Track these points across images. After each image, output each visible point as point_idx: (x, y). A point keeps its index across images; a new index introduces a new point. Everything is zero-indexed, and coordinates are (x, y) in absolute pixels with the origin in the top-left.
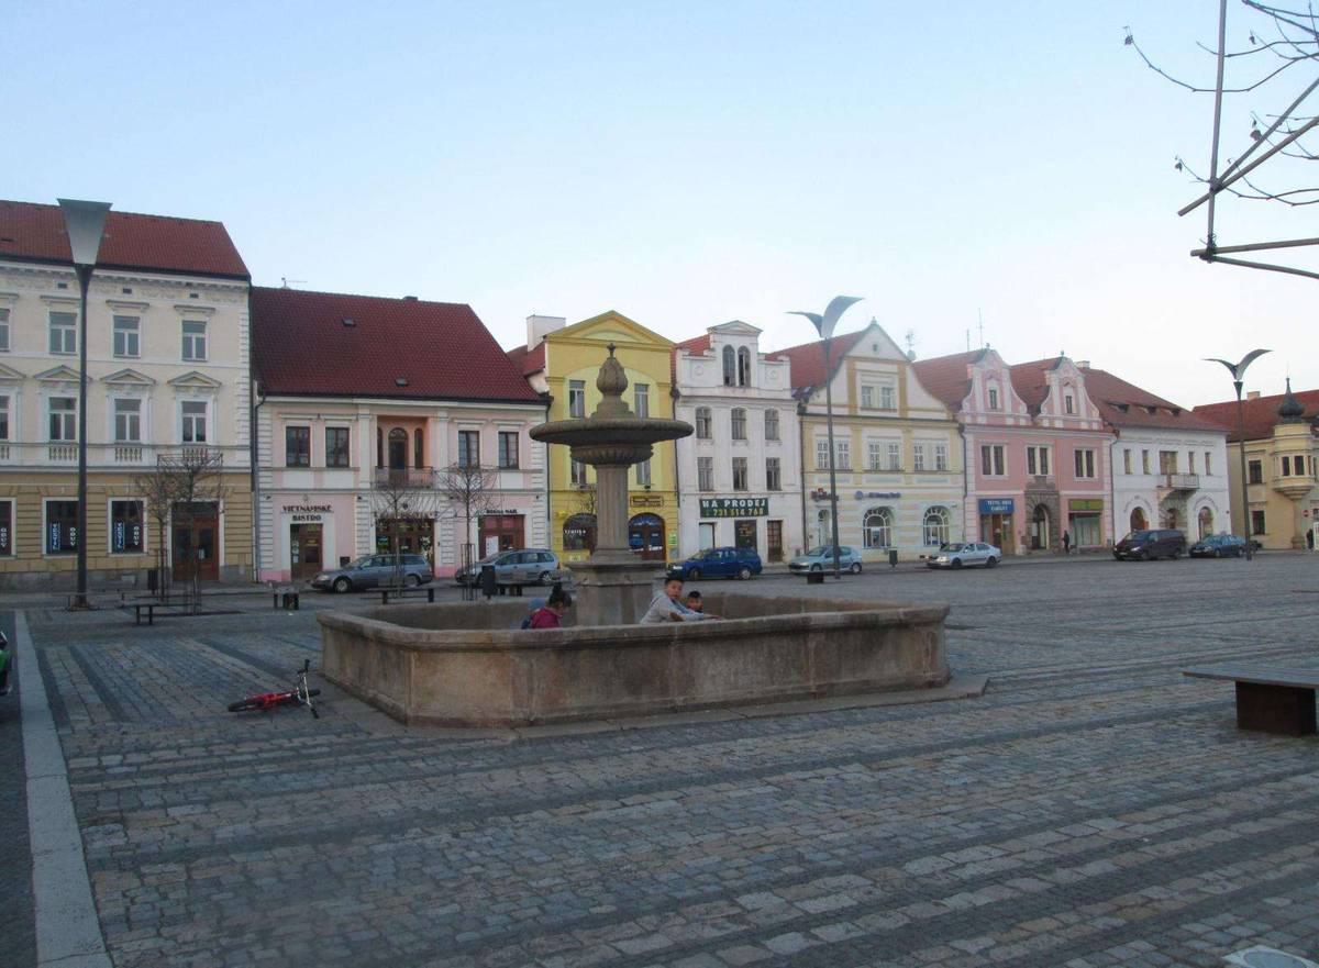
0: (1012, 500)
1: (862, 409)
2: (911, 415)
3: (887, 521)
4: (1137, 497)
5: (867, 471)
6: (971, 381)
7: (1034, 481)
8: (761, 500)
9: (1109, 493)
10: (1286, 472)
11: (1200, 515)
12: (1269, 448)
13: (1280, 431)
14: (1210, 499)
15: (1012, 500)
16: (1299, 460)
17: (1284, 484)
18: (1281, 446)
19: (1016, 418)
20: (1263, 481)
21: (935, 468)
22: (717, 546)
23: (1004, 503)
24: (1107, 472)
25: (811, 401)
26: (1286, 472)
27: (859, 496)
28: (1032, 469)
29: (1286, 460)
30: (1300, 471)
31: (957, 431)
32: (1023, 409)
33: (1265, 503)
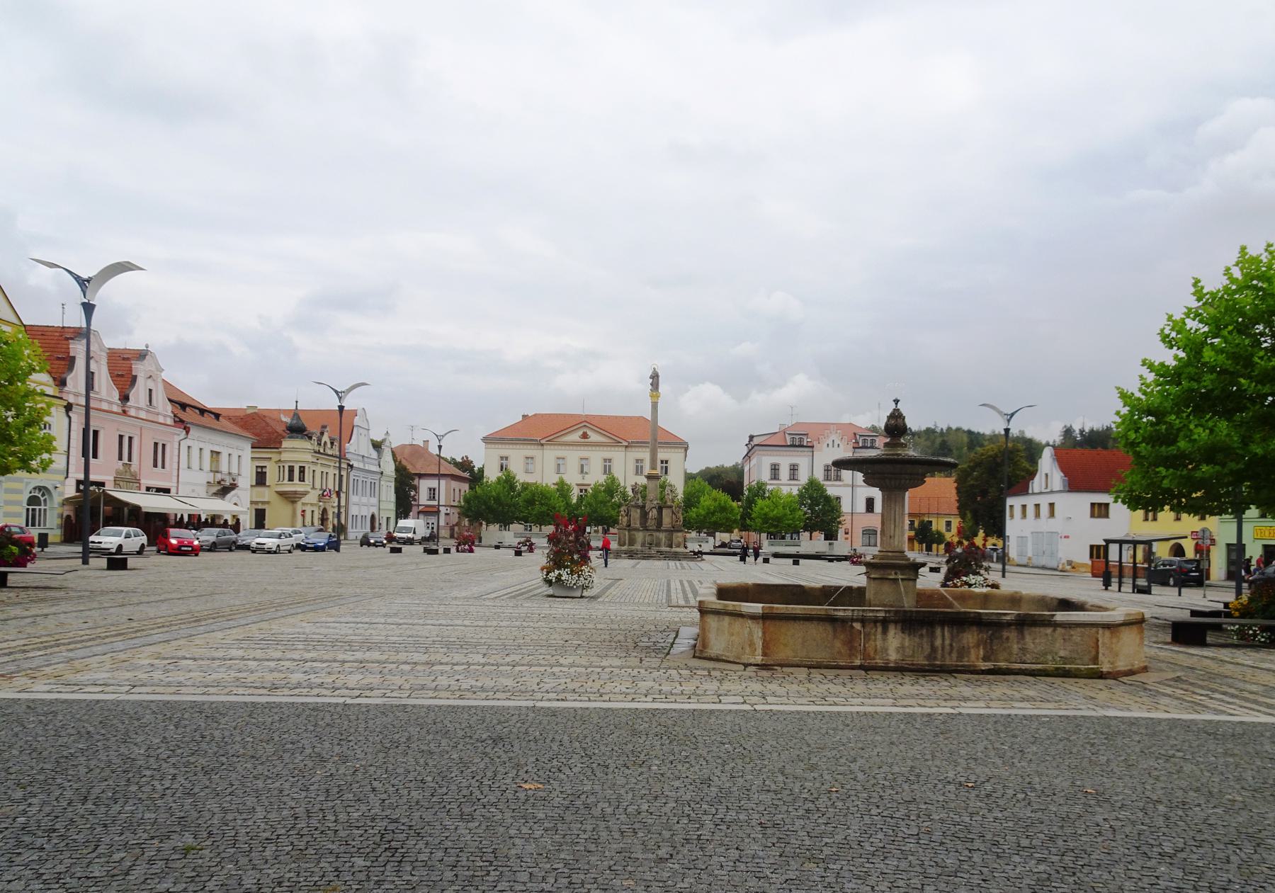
3: (45, 500)
6: (74, 358)
7: (121, 468)
9: (176, 485)
10: (291, 479)
12: (275, 457)
13: (287, 444)
16: (302, 470)
17: (288, 487)
18: (285, 456)
19: (111, 403)
20: (267, 484)
22: (1177, 589)
26: (291, 479)
28: (120, 458)
29: (291, 470)
30: (302, 479)
31: (64, 410)
32: (116, 395)
33: (268, 503)
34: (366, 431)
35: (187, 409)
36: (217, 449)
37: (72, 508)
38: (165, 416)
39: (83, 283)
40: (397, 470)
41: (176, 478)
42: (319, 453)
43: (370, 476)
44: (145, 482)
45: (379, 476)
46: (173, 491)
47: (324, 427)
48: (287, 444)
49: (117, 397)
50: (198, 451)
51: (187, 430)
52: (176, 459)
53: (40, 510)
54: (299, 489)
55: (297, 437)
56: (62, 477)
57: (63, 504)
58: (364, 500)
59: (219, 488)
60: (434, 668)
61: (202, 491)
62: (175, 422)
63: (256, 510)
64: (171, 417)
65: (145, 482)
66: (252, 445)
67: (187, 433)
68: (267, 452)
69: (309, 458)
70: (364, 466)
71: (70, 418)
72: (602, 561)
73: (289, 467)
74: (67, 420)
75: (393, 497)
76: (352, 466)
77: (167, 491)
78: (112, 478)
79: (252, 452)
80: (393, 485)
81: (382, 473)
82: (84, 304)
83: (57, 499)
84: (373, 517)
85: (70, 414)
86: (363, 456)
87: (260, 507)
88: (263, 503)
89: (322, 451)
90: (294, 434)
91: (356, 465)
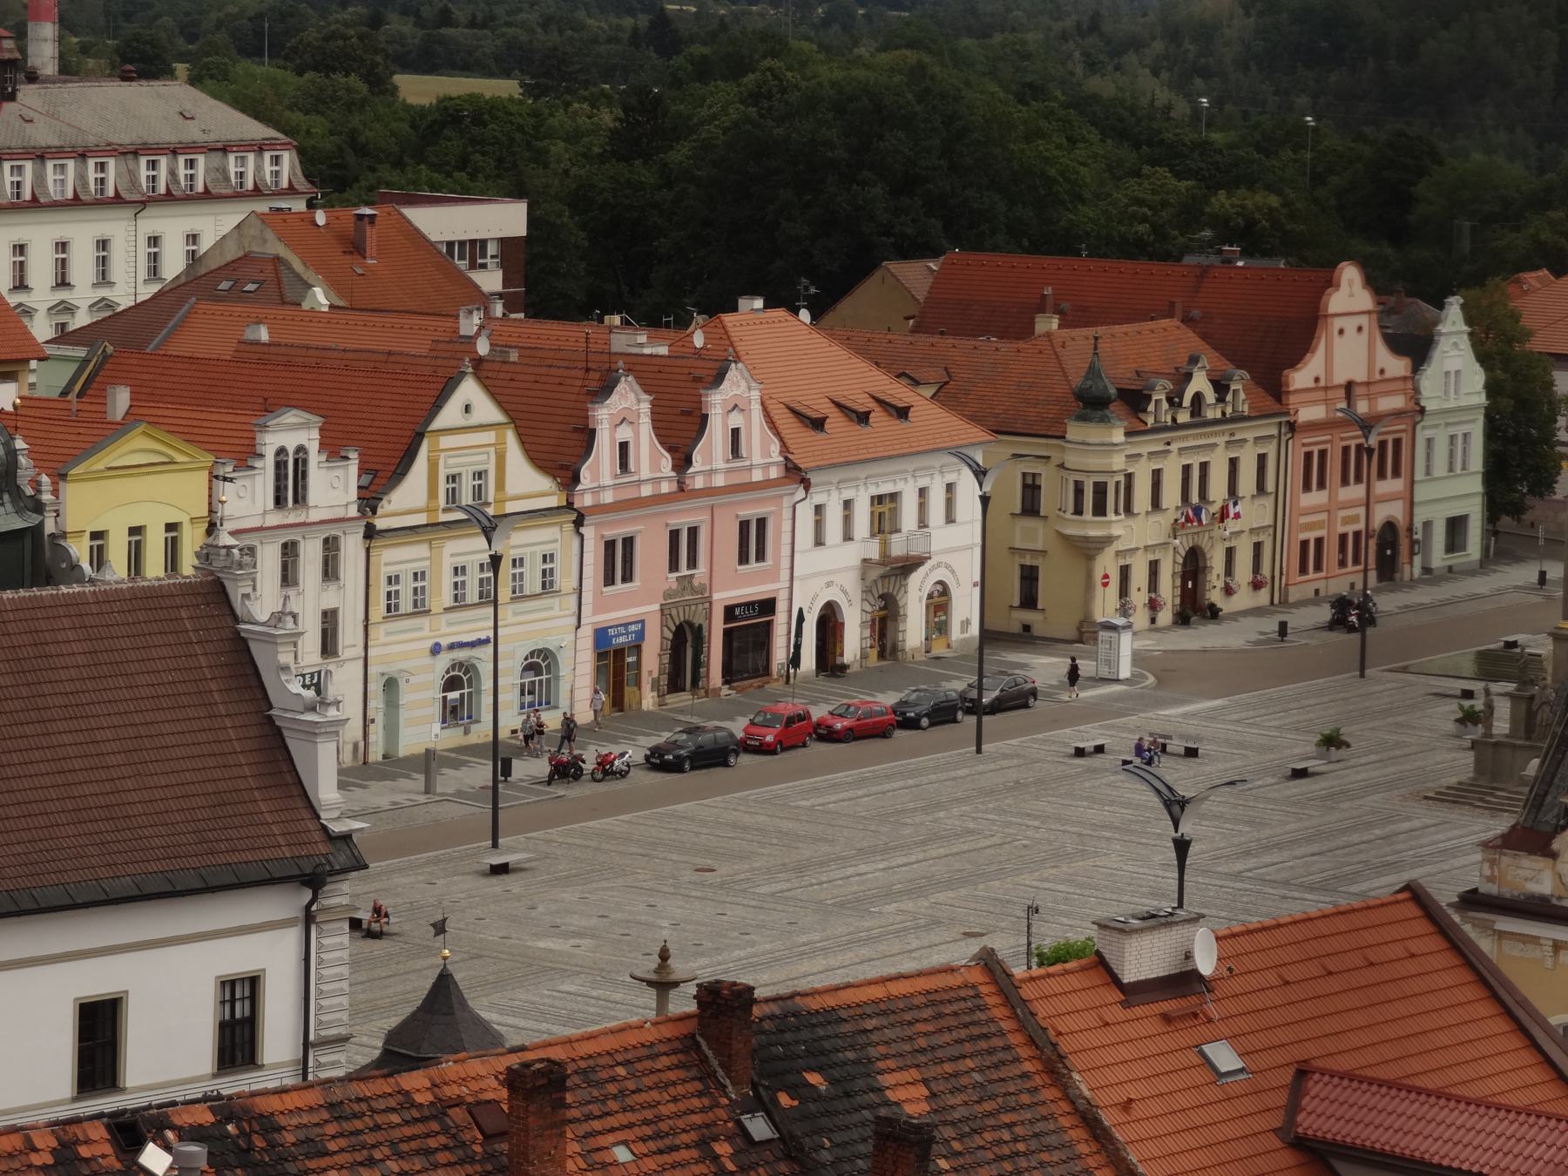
0: (642, 622)
1: (445, 510)
2: (511, 507)
4: (829, 585)
5: (448, 610)
8: (312, 674)
10: (1078, 511)
11: (930, 596)
14: (947, 567)
15: (642, 622)
21: (539, 590)
23: (633, 628)
25: (380, 511)
26: (1078, 511)
27: (436, 650)
28: (674, 565)
30: (1100, 509)
32: (666, 462)
36: (886, 488)
51: (807, 485)
52: (786, 538)
53: (541, 681)
54: (1092, 533)
60: (1240, 203)
63: (1022, 567)
67: (807, 489)
68: (758, 500)
71: (582, 536)
73: (1096, 484)
74: (576, 542)
78: (657, 607)
85: (582, 530)
87: (1028, 561)
88: (1034, 552)
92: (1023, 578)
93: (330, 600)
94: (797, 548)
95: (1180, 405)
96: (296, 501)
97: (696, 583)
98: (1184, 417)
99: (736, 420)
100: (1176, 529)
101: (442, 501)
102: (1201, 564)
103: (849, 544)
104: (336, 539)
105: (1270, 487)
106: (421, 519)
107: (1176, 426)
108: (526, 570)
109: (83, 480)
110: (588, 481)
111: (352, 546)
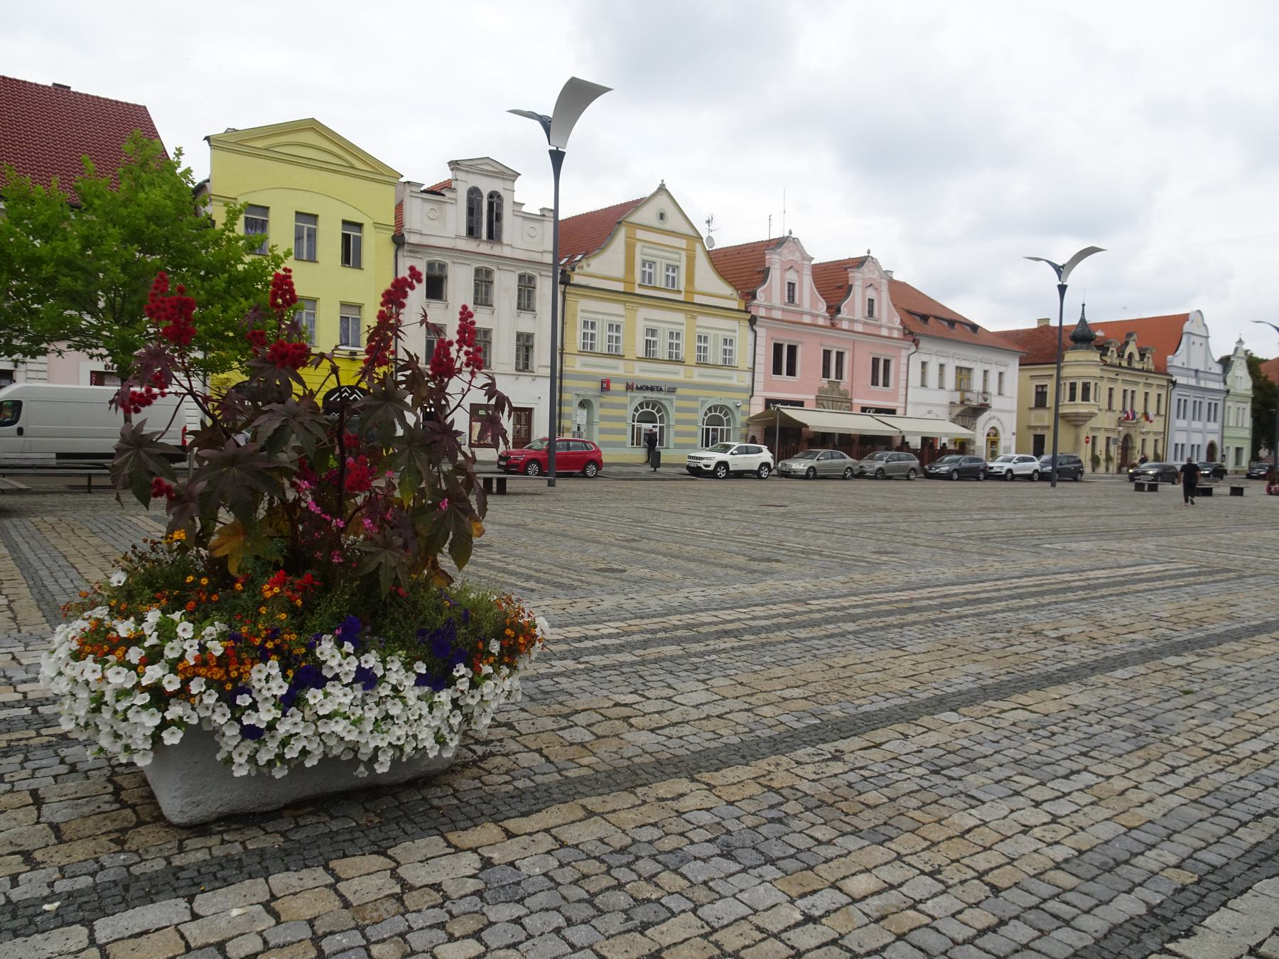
5: (639, 359)
7: (826, 386)
11: (988, 435)
14: (999, 420)
16: (1086, 388)
20: (1048, 405)
24: (903, 384)
28: (826, 373)
29: (1073, 387)
30: (1085, 397)
31: (747, 324)
32: (822, 307)
34: (1203, 340)
35: (957, 325)
36: (965, 364)
37: (760, 428)
38: (890, 329)
39: (1059, 270)
40: (1255, 387)
41: (904, 398)
42: (1120, 366)
43: (1208, 396)
44: (858, 402)
45: (1224, 395)
46: (900, 412)
47: (1130, 335)
48: (1069, 356)
49: (825, 309)
50: (982, 373)
51: (916, 342)
52: (903, 376)
53: (722, 430)
55: (1081, 348)
56: (746, 396)
57: (748, 425)
58: (1197, 425)
59: (962, 408)
61: (943, 413)
62: (904, 334)
64: (898, 329)
65: (858, 402)
66: (1021, 359)
67: (917, 345)
69: (1096, 371)
70: (1198, 382)
71: (755, 332)
72: (508, 918)
74: (751, 335)
75: (1248, 422)
76: (1174, 383)
77: (892, 412)
78: (814, 397)
79: (1020, 370)
80: (1248, 407)
81: (1228, 391)
82: (1059, 286)
83: (740, 419)
84: (1212, 447)
86: (1197, 371)
87: (1039, 432)
88: (1043, 428)
89: (1124, 364)
90: (1079, 345)
91: (1181, 380)
92: (1035, 442)
93: (525, 324)
94: (910, 384)
95: (1123, 357)
96: (490, 236)
97: (841, 388)
98: (1124, 364)
99: (871, 294)
100: (1120, 422)
101: (638, 279)
102: (1130, 445)
103: (941, 392)
104: (531, 279)
105: (1163, 412)
106: (620, 287)
107: (1120, 366)
108: (710, 345)
109: (259, 156)
110: (763, 299)
111: (544, 287)
